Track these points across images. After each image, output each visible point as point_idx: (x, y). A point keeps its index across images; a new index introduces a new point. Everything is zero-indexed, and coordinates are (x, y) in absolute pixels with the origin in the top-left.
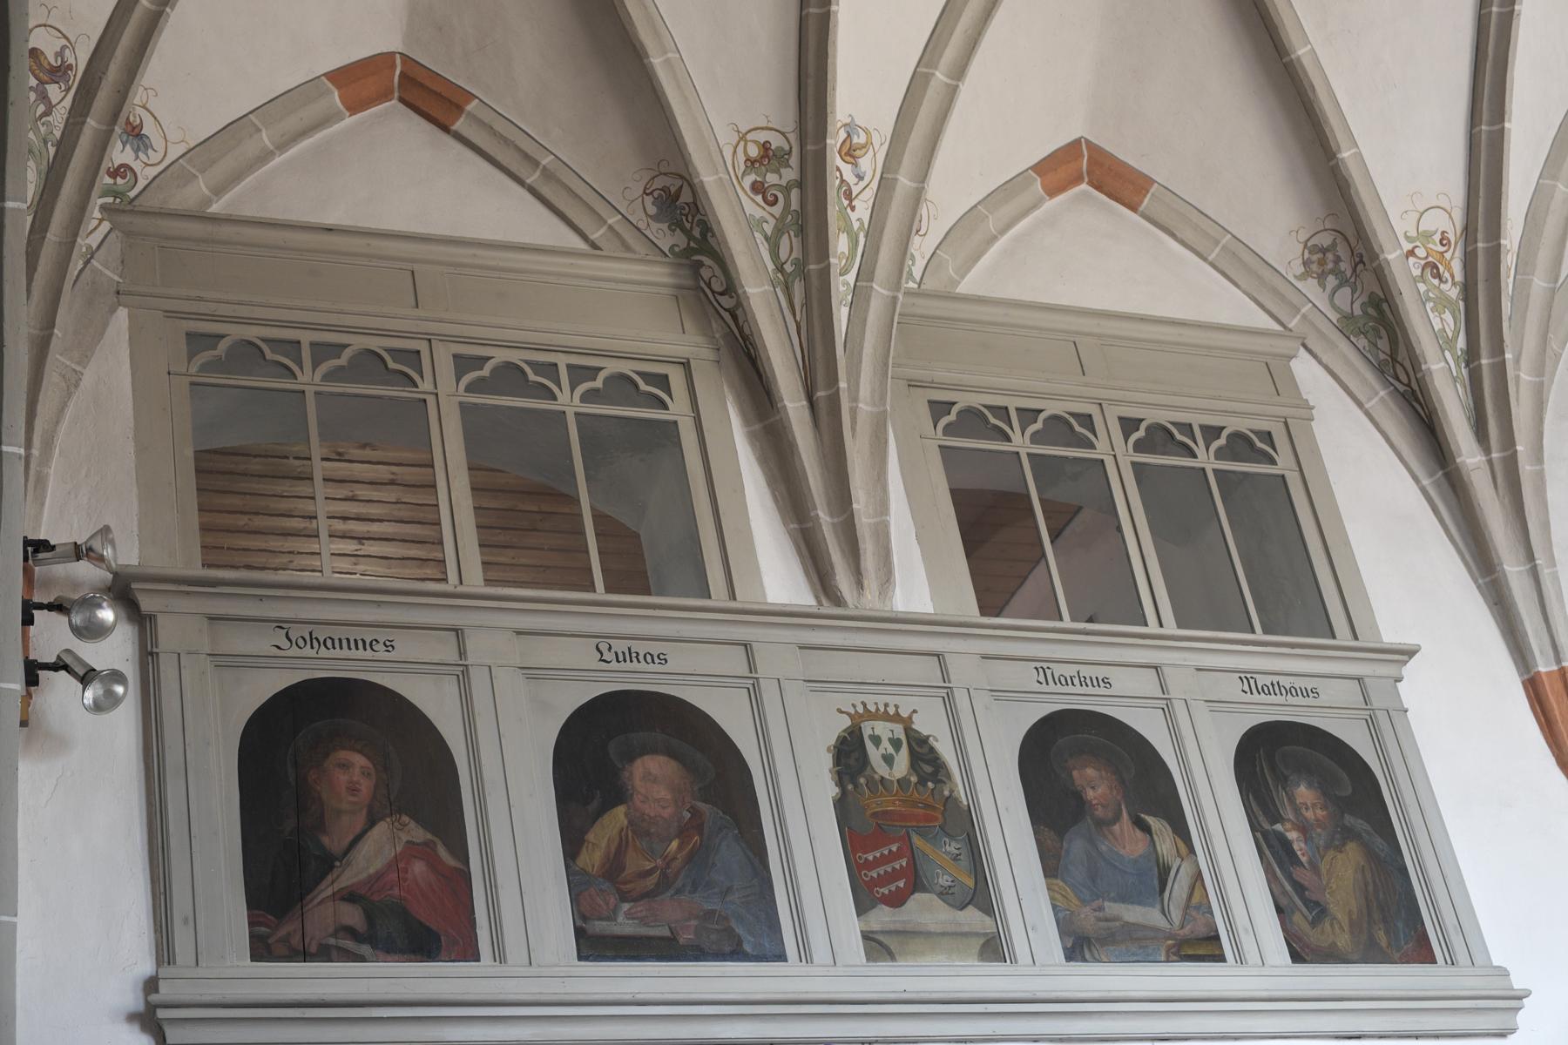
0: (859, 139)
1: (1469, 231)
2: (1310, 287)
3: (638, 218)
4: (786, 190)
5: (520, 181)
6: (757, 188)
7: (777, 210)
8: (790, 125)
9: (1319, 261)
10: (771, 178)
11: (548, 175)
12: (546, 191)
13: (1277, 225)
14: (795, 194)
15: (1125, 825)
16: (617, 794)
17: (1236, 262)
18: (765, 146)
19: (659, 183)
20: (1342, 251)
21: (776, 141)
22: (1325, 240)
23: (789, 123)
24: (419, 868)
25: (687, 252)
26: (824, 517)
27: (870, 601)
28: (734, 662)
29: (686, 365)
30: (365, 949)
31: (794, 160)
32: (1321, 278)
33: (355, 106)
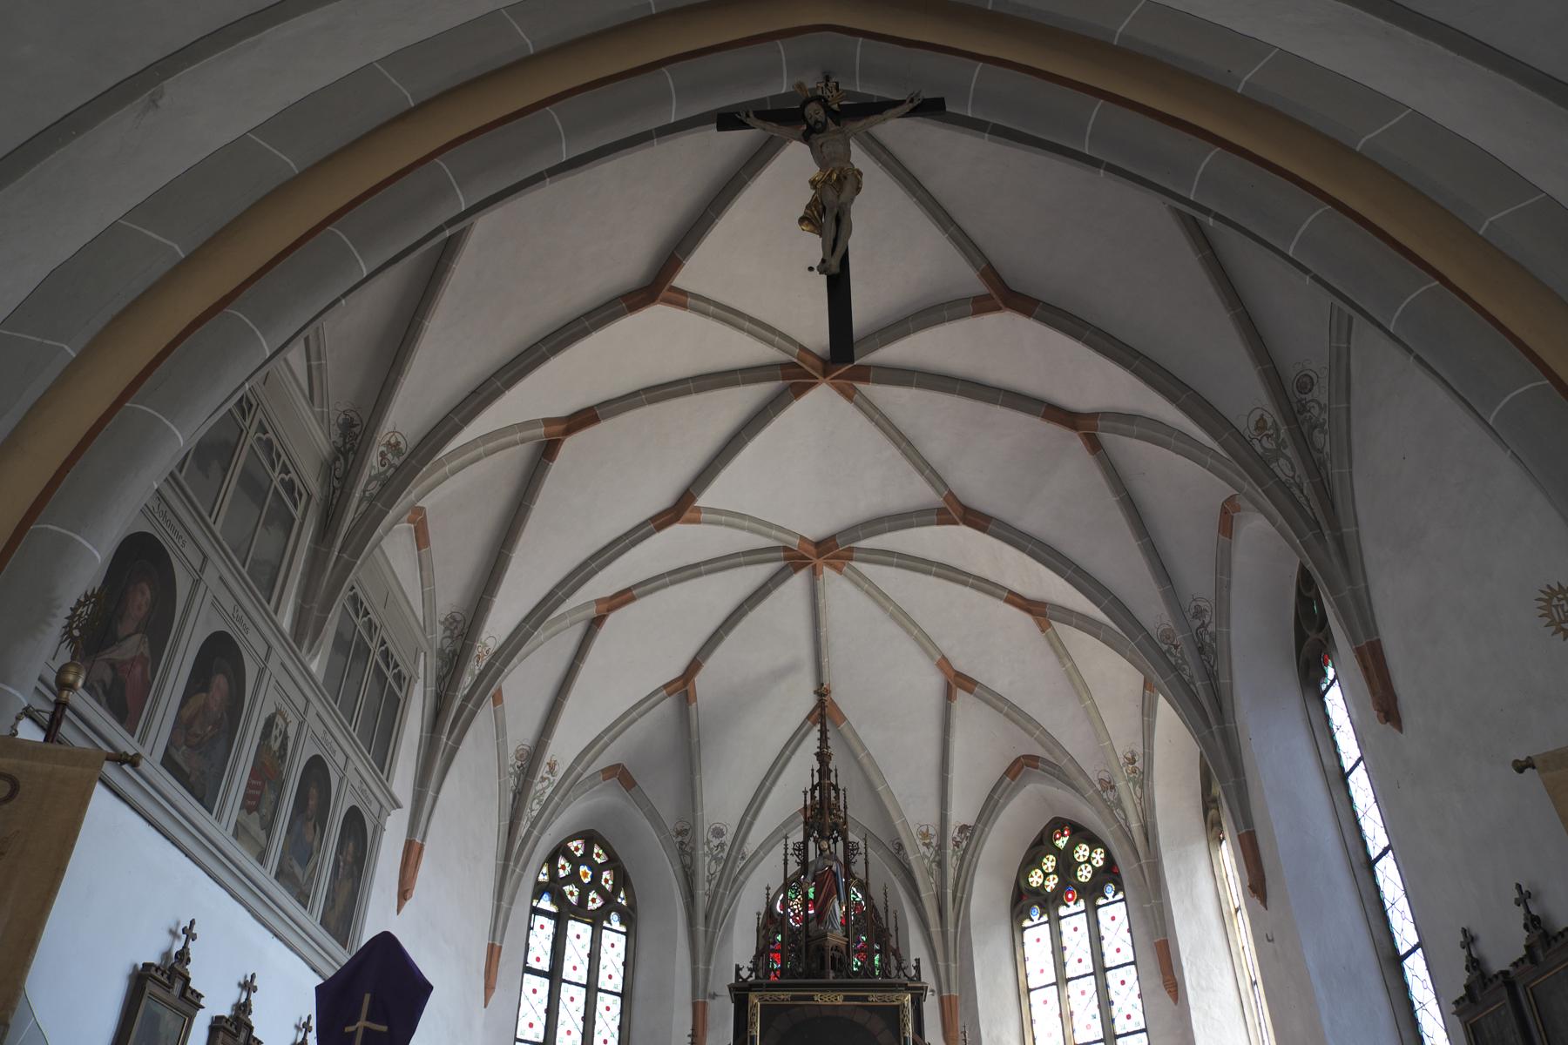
0: (924, 829)
1: (496, 655)
2: (440, 628)
3: (333, 418)
4: (391, 466)
5: (308, 360)
6: (383, 455)
7: (382, 469)
8: (412, 445)
9: (451, 622)
10: (390, 456)
11: (320, 366)
12: (315, 373)
13: (451, 595)
14: (392, 471)
15: (311, 824)
16: (206, 688)
17: (429, 599)
18: (398, 443)
19: (352, 414)
20: (460, 626)
21: (403, 445)
22: (459, 618)
23: (413, 444)
24: (138, 670)
25: (338, 449)
26: (701, 966)
27: (303, 654)
28: (262, 652)
29: (310, 496)
30: (104, 699)
31: (402, 458)
32: (446, 629)
33: (939, 664)
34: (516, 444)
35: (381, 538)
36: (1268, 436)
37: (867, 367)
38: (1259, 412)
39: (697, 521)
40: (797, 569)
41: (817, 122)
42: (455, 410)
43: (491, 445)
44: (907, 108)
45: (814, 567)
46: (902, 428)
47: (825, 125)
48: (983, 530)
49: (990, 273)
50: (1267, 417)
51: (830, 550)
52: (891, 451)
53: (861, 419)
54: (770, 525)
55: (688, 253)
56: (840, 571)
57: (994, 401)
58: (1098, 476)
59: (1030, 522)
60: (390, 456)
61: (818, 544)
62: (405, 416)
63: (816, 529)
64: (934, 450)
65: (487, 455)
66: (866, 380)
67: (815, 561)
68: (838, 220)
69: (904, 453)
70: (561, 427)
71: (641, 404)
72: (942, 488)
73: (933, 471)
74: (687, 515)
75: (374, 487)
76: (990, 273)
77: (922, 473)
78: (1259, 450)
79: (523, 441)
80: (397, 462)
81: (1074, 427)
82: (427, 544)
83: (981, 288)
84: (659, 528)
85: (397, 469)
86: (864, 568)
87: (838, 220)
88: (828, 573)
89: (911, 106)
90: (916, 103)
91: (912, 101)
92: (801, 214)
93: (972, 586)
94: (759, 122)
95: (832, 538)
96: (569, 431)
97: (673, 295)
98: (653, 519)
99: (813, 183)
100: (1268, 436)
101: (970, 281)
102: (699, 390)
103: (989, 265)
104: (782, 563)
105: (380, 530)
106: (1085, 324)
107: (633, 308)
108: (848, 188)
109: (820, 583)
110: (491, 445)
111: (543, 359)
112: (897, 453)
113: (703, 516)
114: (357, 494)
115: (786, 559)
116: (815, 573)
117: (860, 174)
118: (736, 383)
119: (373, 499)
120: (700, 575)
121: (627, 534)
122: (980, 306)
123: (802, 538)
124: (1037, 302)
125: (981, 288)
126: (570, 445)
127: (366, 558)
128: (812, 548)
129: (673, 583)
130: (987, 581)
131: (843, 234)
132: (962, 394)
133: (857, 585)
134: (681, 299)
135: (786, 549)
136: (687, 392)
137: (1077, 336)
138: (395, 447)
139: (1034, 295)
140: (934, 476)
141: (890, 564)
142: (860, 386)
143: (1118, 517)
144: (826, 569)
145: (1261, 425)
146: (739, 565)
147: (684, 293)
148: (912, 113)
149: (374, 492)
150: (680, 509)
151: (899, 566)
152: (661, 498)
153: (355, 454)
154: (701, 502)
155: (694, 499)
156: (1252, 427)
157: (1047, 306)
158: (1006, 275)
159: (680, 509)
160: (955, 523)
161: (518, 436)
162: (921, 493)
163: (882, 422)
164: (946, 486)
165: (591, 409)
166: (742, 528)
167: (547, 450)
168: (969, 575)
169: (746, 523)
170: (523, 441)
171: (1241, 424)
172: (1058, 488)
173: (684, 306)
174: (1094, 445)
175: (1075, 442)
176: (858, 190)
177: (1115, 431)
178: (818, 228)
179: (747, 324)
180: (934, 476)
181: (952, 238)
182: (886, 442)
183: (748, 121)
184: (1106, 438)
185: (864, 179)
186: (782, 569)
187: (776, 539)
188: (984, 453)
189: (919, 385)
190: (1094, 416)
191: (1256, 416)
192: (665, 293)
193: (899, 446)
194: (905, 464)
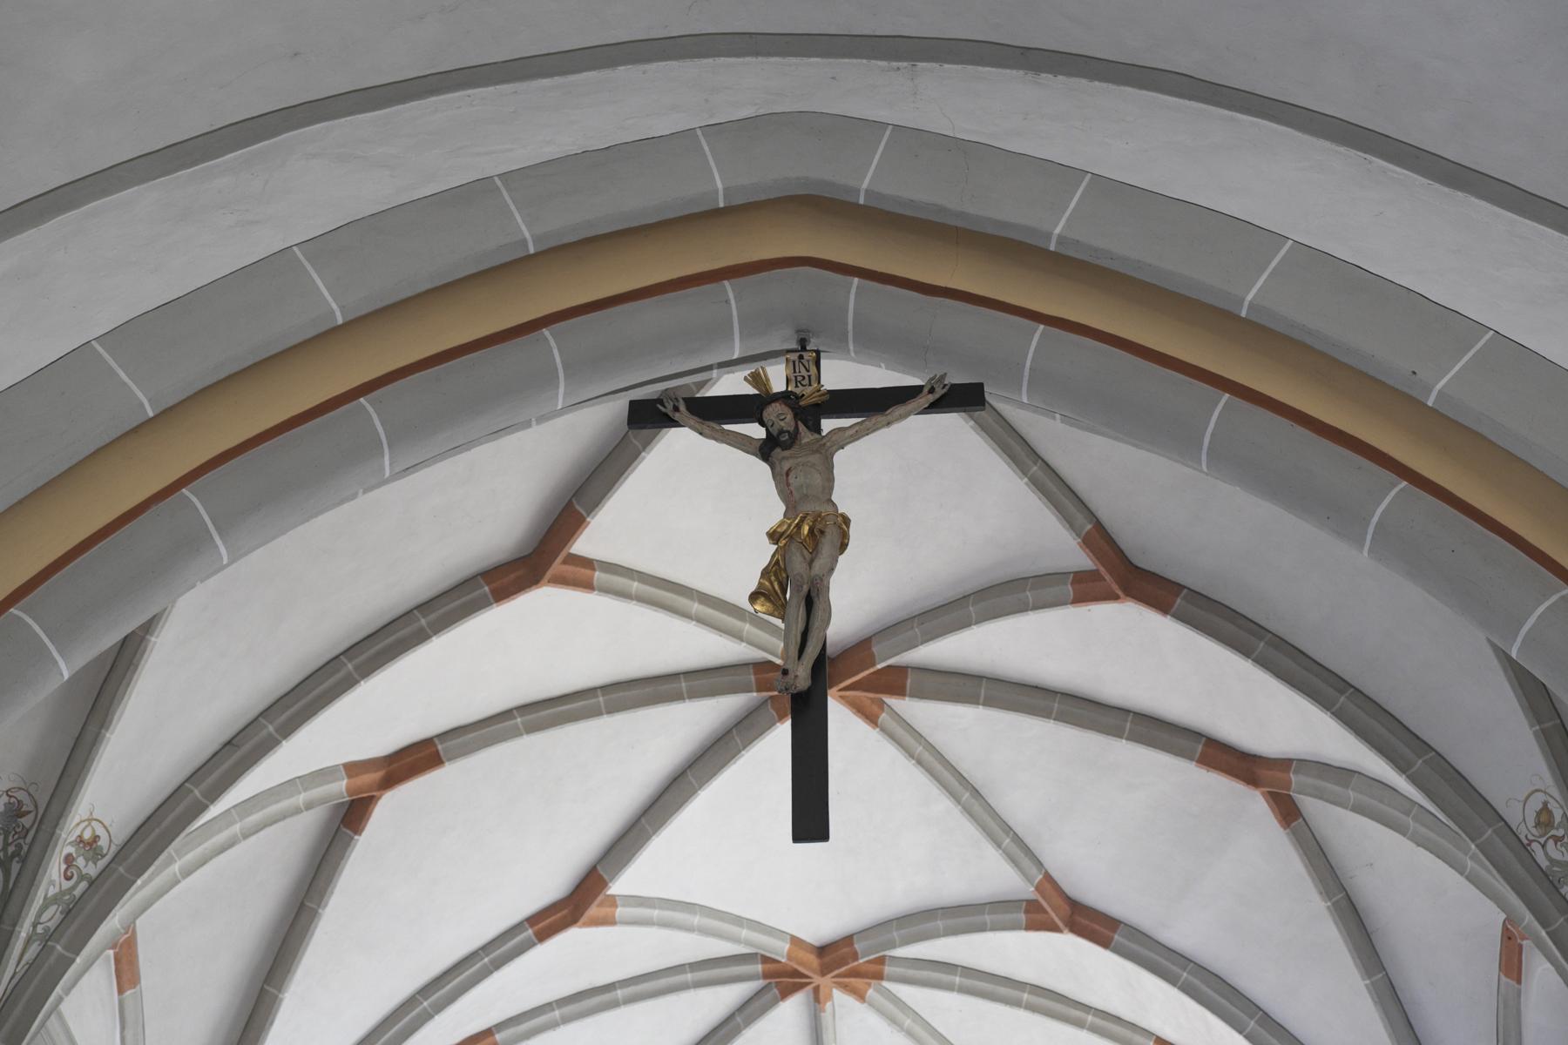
4: (82, 877)
6: (69, 860)
7: (67, 885)
8: (120, 839)
10: (80, 862)
14: (83, 885)
18: (96, 838)
19: (21, 795)
21: (103, 843)
23: (120, 837)
31: (102, 863)
34: (297, 811)
35: (60, 1000)
36: (1557, 839)
37: (901, 671)
38: (1540, 797)
39: (609, 921)
40: (786, 993)
41: (781, 432)
42: (196, 776)
43: (255, 818)
44: (925, 400)
45: (816, 990)
46: (964, 768)
47: (794, 436)
48: (1104, 943)
49: (1099, 538)
50: (1552, 805)
51: (842, 962)
52: (943, 804)
53: (890, 751)
54: (738, 921)
55: (595, 504)
56: (861, 996)
57: (1117, 733)
58: (1293, 862)
59: (1184, 933)
60: (80, 862)
61: (822, 950)
62: (109, 797)
63: (820, 927)
64: (1020, 804)
65: (246, 836)
66: (900, 691)
67: (817, 980)
68: (809, 603)
69: (968, 811)
70: (376, 776)
71: (515, 733)
72: (1033, 871)
73: (1018, 840)
74: (593, 911)
75: (52, 916)
76: (1099, 538)
77: (998, 845)
78: (1544, 863)
79: (309, 806)
80: (92, 870)
81: (1252, 780)
82: (135, 980)
83: (1083, 561)
84: (542, 936)
85: (92, 883)
86: (904, 992)
87: (809, 603)
88: (841, 1000)
89: (931, 398)
90: (939, 392)
91: (932, 391)
92: (753, 587)
93: (1094, 1029)
94: (693, 420)
95: (848, 940)
96: (390, 782)
97: (569, 570)
98: (532, 920)
99: (774, 536)
100: (1557, 839)
101: (1066, 550)
102: (613, 709)
103: (1099, 526)
104: (760, 983)
105: (58, 990)
106: (1258, 630)
107: (503, 593)
108: (826, 548)
109: (826, 1017)
110: (255, 818)
111: (348, 684)
112: (956, 811)
113: (620, 912)
114: (24, 932)
115: (766, 976)
116: (817, 998)
117: (847, 521)
118: (677, 697)
119: (50, 937)
120: (615, 1004)
121: (486, 948)
122: (1085, 589)
123: (796, 941)
124: (1175, 588)
125: (1083, 561)
126: (389, 806)
127: (32, 1039)
128: (812, 959)
129: (566, 1020)
130: (1118, 1020)
131: (816, 623)
132: (1063, 718)
133: (893, 1021)
134: (583, 575)
135: (766, 960)
136: (595, 713)
137: (1244, 650)
138: (90, 846)
139: (1171, 575)
140: (1017, 848)
141: (949, 987)
142: (892, 701)
143: (1330, 933)
144: (837, 994)
145: (1544, 819)
146: (684, 987)
147: (587, 563)
148: (936, 407)
149: (52, 925)
150: (581, 900)
151: (963, 990)
152: (551, 884)
153: (23, 861)
154: (621, 886)
155: (603, 884)
156: (1531, 822)
157: (1197, 597)
158: (1129, 538)
159: (581, 900)
160: (1054, 928)
161: (301, 799)
162: (997, 876)
163: (927, 756)
164: (1039, 864)
165: (427, 743)
166: (689, 929)
167: (352, 815)
168: (1087, 1008)
169: (696, 920)
170: (309, 806)
171: (1513, 815)
172: (1228, 880)
173: (588, 586)
174: (1287, 811)
175: (1255, 803)
176: (843, 547)
177: (1320, 795)
178: (780, 608)
179: (696, 607)
180: (1017, 848)
181: (1036, 483)
182: (934, 790)
183: (677, 416)
184: (1310, 805)
185: (854, 531)
186: (759, 993)
187: (748, 943)
188: (1103, 815)
189: (990, 702)
190: (1285, 764)
191: (1535, 804)
192: (557, 567)
193: (956, 799)
194: (969, 829)
